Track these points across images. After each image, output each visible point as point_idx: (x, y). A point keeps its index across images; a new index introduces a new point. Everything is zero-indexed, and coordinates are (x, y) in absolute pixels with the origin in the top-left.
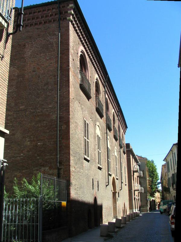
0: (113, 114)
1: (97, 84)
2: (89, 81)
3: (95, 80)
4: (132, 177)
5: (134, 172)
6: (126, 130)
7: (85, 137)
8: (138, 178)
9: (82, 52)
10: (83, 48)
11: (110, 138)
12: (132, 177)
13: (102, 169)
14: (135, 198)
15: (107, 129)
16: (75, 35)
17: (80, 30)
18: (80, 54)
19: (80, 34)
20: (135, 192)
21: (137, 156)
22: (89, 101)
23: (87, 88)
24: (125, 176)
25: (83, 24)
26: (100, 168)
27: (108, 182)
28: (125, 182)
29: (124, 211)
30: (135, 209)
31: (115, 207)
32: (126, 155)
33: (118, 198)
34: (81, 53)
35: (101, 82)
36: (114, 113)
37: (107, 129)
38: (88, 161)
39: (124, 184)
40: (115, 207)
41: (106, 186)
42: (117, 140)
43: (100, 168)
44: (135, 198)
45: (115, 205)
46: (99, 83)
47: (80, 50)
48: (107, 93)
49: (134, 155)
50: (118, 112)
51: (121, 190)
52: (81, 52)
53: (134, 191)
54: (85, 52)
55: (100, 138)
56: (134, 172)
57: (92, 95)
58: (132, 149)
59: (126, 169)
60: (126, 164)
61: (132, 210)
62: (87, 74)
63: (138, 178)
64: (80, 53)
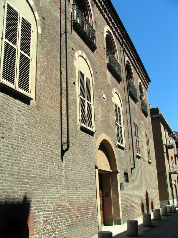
0: (139, 84)
1: (140, 86)
2: (135, 86)
3: (139, 84)
4: (165, 154)
5: (168, 148)
6: (148, 83)
7: (136, 137)
8: (177, 157)
9: (108, 31)
10: (128, 58)
11: (88, 57)
12: (165, 154)
13: (94, 134)
14: (171, 185)
15: (73, 29)
16: (135, 72)
17: (109, 18)
18: (106, 34)
19: (106, 16)
20: (172, 175)
21: (174, 132)
22: (120, 83)
23: (117, 69)
24: (148, 150)
25: (118, 23)
26: (150, 163)
27: (134, 164)
28: (149, 158)
29: (146, 205)
30: (173, 198)
31: (116, 200)
32: (149, 117)
33: (125, 184)
34: (107, 33)
35: (133, 68)
36: (140, 83)
37: (129, 96)
38: (122, 148)
39: (144, 160)
40: (116, 200)
41: (132, 169)
42: (148, 115)
43: (150, 163)
44: (171, 185)
45: (115, 198)
46: (141, 86)
47: (105, 30)
48: (126, 53)
49: (171, 131)
50: (122, 39)
51: (134, 168)
52: (107, 32)
53: (170, 174)
54: (130, 62)
55: (88, 81)
56: (168, 148)
57: (148, 114)
58: (161, 115)
59: (151, 140)
60: (150, 132)
61: (167, 201)
62: (89, 18)
63: (177, 157)
64: (105, 34)
